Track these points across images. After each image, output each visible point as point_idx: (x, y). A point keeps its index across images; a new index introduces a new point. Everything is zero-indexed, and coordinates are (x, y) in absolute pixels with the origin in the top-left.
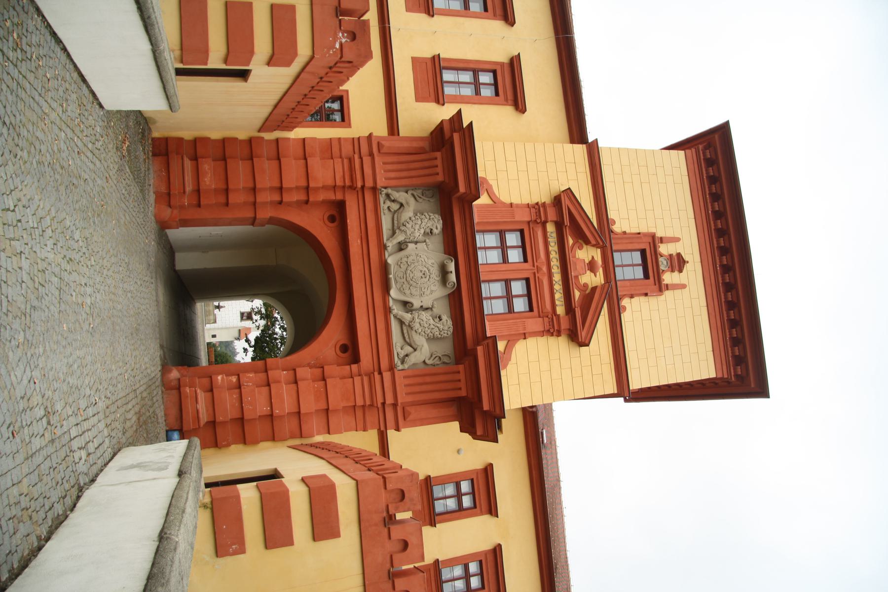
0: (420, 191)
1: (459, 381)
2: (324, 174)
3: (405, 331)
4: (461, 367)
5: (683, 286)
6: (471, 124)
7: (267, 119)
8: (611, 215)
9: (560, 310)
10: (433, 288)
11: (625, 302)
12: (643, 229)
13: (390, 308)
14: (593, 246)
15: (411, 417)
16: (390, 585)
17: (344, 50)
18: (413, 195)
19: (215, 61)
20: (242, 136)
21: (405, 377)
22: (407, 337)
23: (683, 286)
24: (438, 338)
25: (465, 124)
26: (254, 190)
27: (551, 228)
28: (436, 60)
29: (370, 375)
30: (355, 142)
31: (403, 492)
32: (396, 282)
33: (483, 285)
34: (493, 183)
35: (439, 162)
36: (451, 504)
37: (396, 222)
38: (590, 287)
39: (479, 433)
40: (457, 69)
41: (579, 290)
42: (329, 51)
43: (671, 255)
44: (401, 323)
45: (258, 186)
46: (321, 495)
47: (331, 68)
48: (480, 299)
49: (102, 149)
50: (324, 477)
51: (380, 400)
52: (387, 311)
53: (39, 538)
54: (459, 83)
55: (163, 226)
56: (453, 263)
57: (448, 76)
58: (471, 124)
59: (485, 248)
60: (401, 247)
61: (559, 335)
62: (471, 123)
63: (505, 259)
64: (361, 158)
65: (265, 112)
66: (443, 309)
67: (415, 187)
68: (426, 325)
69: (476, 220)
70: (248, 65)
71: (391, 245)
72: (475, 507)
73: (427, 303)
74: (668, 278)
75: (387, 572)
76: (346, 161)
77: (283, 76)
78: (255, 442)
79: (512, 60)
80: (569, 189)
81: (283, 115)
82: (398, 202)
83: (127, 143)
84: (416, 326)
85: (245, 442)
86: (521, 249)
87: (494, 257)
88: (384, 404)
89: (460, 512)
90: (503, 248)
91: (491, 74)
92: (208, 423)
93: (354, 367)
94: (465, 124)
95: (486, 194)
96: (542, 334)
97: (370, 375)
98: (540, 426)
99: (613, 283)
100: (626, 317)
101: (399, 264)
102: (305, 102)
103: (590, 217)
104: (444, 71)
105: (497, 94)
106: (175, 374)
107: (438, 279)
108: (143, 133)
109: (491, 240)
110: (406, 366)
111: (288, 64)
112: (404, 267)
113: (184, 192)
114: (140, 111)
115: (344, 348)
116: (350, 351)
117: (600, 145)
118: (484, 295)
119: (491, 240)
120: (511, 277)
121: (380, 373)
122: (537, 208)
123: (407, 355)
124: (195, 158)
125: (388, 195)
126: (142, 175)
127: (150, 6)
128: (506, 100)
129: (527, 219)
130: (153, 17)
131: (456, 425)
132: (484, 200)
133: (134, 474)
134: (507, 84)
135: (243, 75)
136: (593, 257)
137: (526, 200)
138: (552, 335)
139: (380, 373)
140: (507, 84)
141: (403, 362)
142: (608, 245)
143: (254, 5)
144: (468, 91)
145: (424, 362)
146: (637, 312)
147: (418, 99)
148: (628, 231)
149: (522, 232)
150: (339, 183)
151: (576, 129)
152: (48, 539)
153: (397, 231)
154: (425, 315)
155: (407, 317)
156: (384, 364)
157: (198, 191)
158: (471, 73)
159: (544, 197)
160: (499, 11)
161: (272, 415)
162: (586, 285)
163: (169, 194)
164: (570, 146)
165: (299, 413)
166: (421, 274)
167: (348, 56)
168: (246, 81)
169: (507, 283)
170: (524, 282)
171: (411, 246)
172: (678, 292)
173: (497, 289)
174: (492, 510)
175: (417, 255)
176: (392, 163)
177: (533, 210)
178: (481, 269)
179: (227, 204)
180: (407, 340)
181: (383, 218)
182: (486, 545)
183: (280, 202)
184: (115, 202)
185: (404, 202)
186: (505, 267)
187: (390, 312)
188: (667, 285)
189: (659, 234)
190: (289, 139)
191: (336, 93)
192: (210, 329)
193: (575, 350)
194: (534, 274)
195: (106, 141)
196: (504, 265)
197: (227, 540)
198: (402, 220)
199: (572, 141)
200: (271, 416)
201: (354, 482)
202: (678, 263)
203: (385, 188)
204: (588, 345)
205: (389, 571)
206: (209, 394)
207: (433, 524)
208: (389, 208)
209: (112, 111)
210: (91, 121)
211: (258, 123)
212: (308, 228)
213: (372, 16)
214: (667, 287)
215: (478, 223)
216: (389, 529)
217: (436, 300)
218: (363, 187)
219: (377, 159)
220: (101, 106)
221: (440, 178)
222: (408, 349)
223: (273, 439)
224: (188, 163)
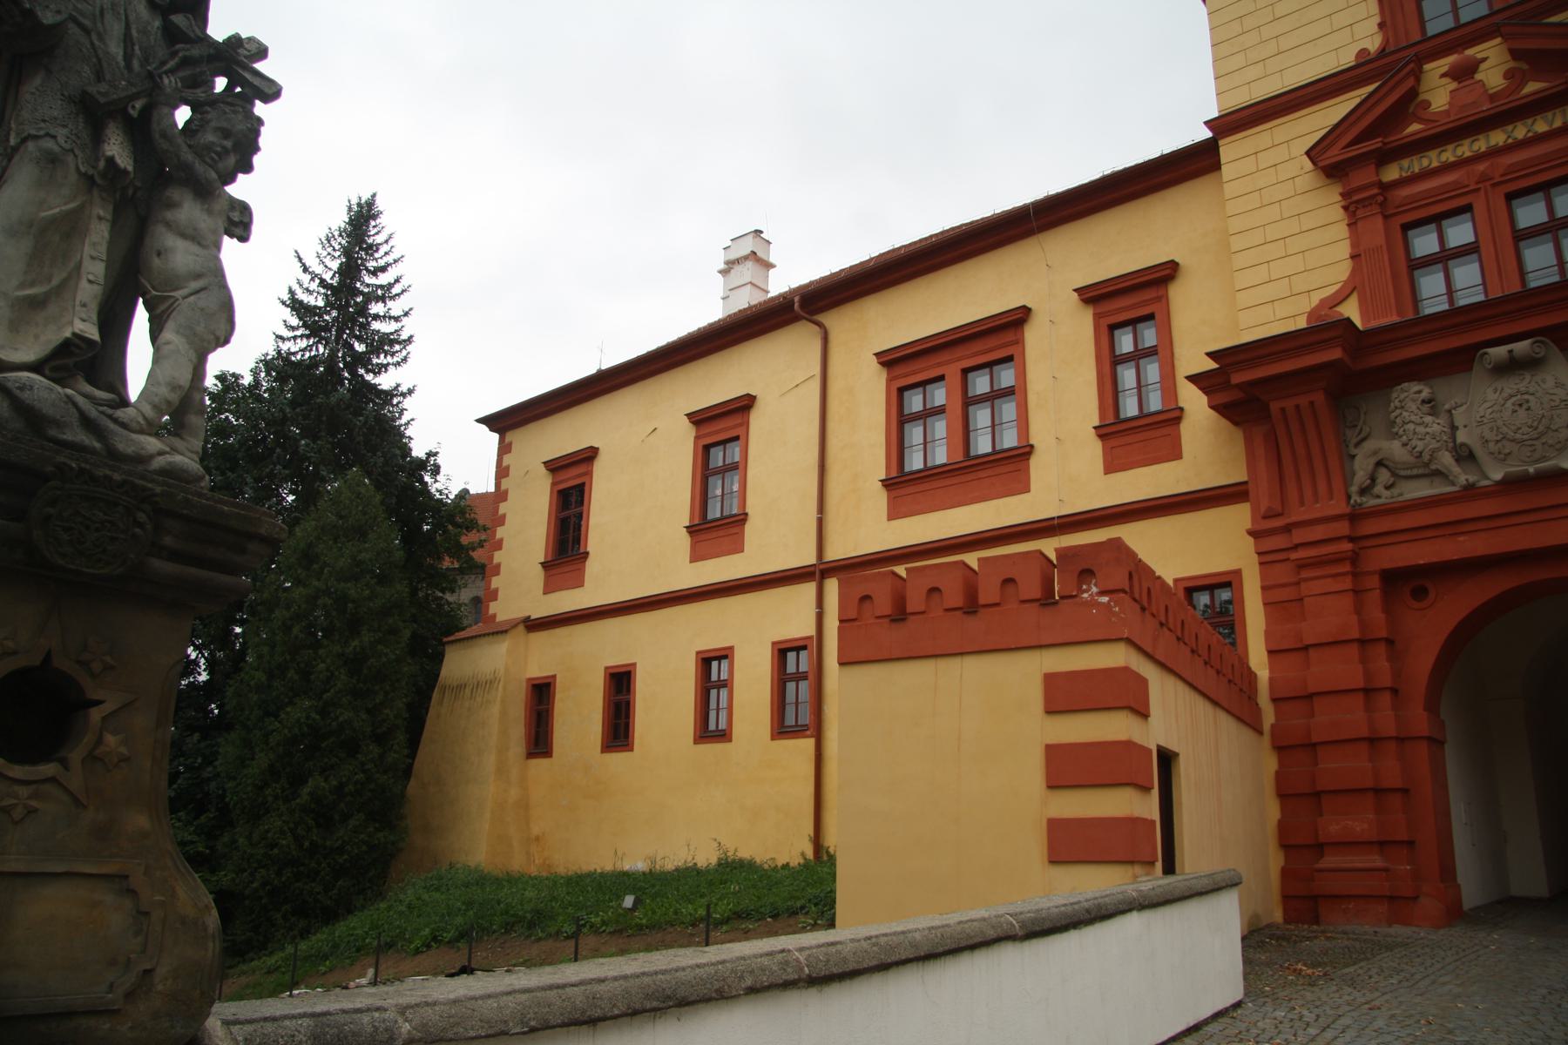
0: (1349, 433)
2: (1331, 612)
6: (1211, 355)
7: (1239, 719)
8: (1347, 59)
10: (1550, 382)
14: (1418, 80)
17: (1111, 587)
18: (1357, 445)
19: (1149, 807)
20: (1271, 763)
25: (1211, 365)
26: (1373, 741)
27: (1392, 173)
28: (1103, 432)
30: (1266, 559)
32: (1544, 458)
34: (1316, 298)
35: (1288, 404)
37: (1415, 472)
38: (1512, 64)
41: (1523, 84)
42: (1114, 614)
45: (1365, 733)
47: (1143, 609)
49: (1316, 1011)
54: (925, 443)
55: (1455, 914)
56: (1491, 351)
57: (1130, 408)
58: (1211, 355)
59: (1450, 292)
60: (1466, 456)
62: (1208, 354)
64: (1296, 547)
65: (1227, 723)
69: (1395, 319)
70: (1150, 751)
71: (1463, 477)
76: (1305, 574)
77: (1163, 690)
80: (1308, 153)
81: (1228, 690)
83: (1300, 966)
87: (1467, 276)
91: (1117, 333)
94: (1211, 365)
95: (1339, 309)
99: (1498, 19)
101: (1503, 458)
103: (1357, 101)
104: (1122, 416)
105: (1150, 317)
107: (1528, 377)
108: (1278, 938)
111: (1143, 682)
112: (1509, 447)
113: (1386, 870)
114: (1244, 939)
117: (1216, 114)
119: (1431, 286)
120: (1508, 230)
122: (1353, 208)
124: (1319, 848)
125: (1363, 491)
126: (1357, 945)
127: (1070, 908)
128: (1159, 299)
129: (1379, 220)
130: (1086, 905)
132: (1351, 310)
134: (1129, 305)
135: (1167, 759)
136: (1443, 75)
137: (1341, 230)
142: (1412, 52)
143: (1050, 742)
144: (1152, 371)
147: (1026, 489)
148: (1377, 19)
149: (1406, 227)
150: (1347, 583)
151: (1194, 163)
153: (1433, 467)
157: (1382, 845)
158: (1119, 368)
160: (1009, 336)
162: (1508, 75)
163: (1392, 899)
164: (1227, 171)
166: (1522, 412)
167: (1120, 580)
168: (1177, 755)
169: (1522, 236)
171: (1461, 437)
175: (1480, 423)
176: (1300, 489)
177: (1360, 213)
178: (1496, 293)
179: (1405, 791)
183: (1394, 691)
184: (1418, 999)
185: (1373, 461)
186: (1487, 249)
190: (1271, 679)
191: (1181, 594)
194: (1494, 185)
195: (1300, 1002)
196: (1483, 249)
198: (1411, 459)
199: (1216, 166)
203: (1349, 497)
208: (1387, 488)
209: (1245, 988)
210: (1266, 1024)
211: (1247, 734)
212: (1442, 638)
213: (1049, 547)
215: (1399, 314)
218: (1351, 539)
219: (1293, 519)
220: (1238, 1005)
221: (1319, 398)
224: (1330, 861)
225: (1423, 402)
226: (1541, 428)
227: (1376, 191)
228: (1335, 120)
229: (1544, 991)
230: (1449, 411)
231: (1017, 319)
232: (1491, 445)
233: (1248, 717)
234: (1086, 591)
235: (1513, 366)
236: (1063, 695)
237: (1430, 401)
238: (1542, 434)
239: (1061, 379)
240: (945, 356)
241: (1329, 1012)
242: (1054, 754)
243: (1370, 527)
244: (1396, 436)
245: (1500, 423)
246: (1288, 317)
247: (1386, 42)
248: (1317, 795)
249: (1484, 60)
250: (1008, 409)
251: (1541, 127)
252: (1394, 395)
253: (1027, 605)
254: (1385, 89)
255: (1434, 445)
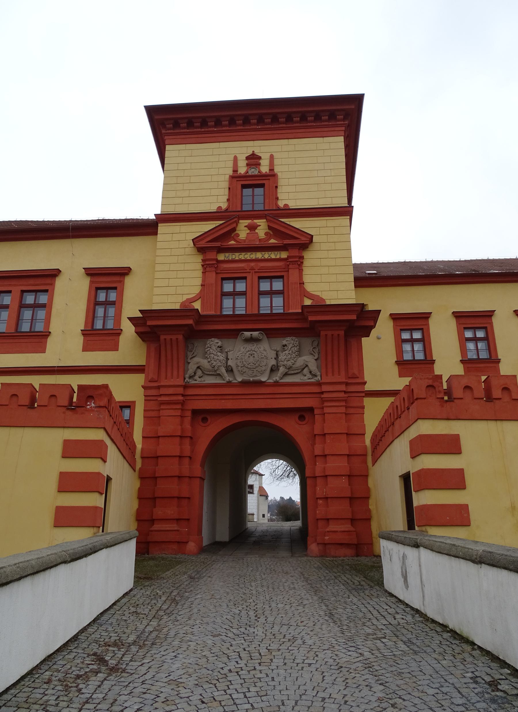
0: (188, 353)
1: (332, 335)
2: (170, 424)
3: (293, 372)
4: (323, 333)
5: (272, 157)
7: (130, 465)
8: (213, 208)
9: (284, 255)
10: (262, 349)
11: (281, 204)
12: (226, 185)
13: (275, 382)
14: (237, 225)
15: (356, 371)
16: (497, 401)
20: (137, 484)
21: (327, 375)
22: (297, 371)
23: (272, 157)
24: (299, 349)
25: (140, 315)
27: (221, 257)
28: (85, 333)
29: (323, 401)
30: (148, 399)
31: (428, 386)
32: (256, 376)
33: (261, 312)
34: (185, 298)
35: (168, 337)
36: (418, 347)
37: (211, 373)
38: (268, 231)
39: (373, 324)
40: (94, 317)
41: (270, 239)
43: (248, 165)
44: (286, 374)
46: (422, 446)
48: (272, 314)
50: (412, 442)
51: (342, 395)
52: (276, 384)
53: (473, 649)
57: (99, 325)
59: (234, 307)
60: (230, 370)
61: (302, 257)
62: (140, 311)
63: (243, 294)
64: (161, 395)
65: (126, 465)
66: (278, 343)
67: (186, 356)
68: (289, 356)
69: (212, 313)
71: (228, 378)
72: (422, 329)
73: (273, 354)
74: (265, 169)
75: (487, 403)
76: (162, 407)
78: (368, 490)
79: (88, 274)
80: (193, 240)
81: (127, 451)
82: (196, 370)
84: (289, 363)
85: (368, 498)
86: (236, 281)
87: (241, 302)
88: (345, 392)
89: (425, 341)
90: (234, 294)
92: (352, 525)
93: (316, 411)
94: (140, 315)
96: (301, 271)
97: (323, 401)
98: (364, 275)
99: (266, 212)
100: (292, 205)
101: (242, 373)
102: (124, 435)
103: (214, 226)
105: (115, 288)
106: (313, 547)
109: (228, 303)
110: (318, 373)
112: (245, 370)
113: (178, 531)
115: (302, 418)
116: (304, 414)
118: (269, 312)
119: (228, 303)
120: (257, 290)
121: (322, 393)
122: (206, 266)
123: (310, 372)
124: (152, 521)
125: (191, 377)
129: (214, 274)
131: (364, 340)
132: (197, 305)
133: (413, 580)
134: (107, 281)
135: (109, 479)
136: (245, 226)
138: (302, 263)
139: (322, 393)
140: (107, 281)
141: (316, 376)
142: (238, 214)
144: (111, 311)
145: (316, 360)
146: (289, 196)
147: (44, 351)
148: (227, 197)
149: (223, 279)
150: (179, 413)
152: (473, 644)
153: (218, 372)
154: (282, 357)
155: (282, 370)
156: (316, 389)
159: (198, 259)
160: (48, 281)
161: (349, 476)
162: (266, 234)
165: (348, 455)
166: (251, 357)
169: (262, 293)
170: (261, 280)
171: (230, 363)
172: (276, 162)
173: (265, 302)
174: (425, 317)
175: (237, 359)
177: (208, 269)
180: (299, 371)
181: (206, 382)
182: (453, 323)
185: (196, 366)
187: (278, 382)
188: (270, 170)
189: (230, 172)
190: (142, 449)
192: (258, 519)
193: (315, 246)
194: (255, 272)
197: (460, 516)
198: (211, 368)
199: (156, 234)
200: (350, 476)
201: (419, 421)
202: (253, 159)
203: (185, 379)
204: (312, 236)
205: (486, 401)
206: (331, 522)
207: (433, 362)
208: (199, 377)
214: (272, 170)
215: (215, 312)
216: (455, 399)
217: (271, 348)
218: (183, 395)
219: (162, 384)
221: (180, 337)
222: (306, 371)
223: (367, 476)
225: (218, 347)
226: (257, 365)
227: (215, 262)
228: (206, 231)
229: (238, 577)
230: (227, 352)
231: (53, 274)
232: (239, 368)
233: (132, 466)
234: (88, 405)
235: (251, 340)
236: (71, 449)
237: (221, 347)
238: (257, 367)
239: (69, 307)
240: (14, 282)
241: (167, 591)
242: (63, 476)
243: (190, 392)
244: (206, 358)
245: (244, 360)
246: (172, 303)
247: (229, 206)
248: (155, 498)
249: (260, 226)
250: (41, 314)
251: (273, 256)
252: (208, 342)
253: (59, 408)
254: (225, 225)
255: (220, 364)
